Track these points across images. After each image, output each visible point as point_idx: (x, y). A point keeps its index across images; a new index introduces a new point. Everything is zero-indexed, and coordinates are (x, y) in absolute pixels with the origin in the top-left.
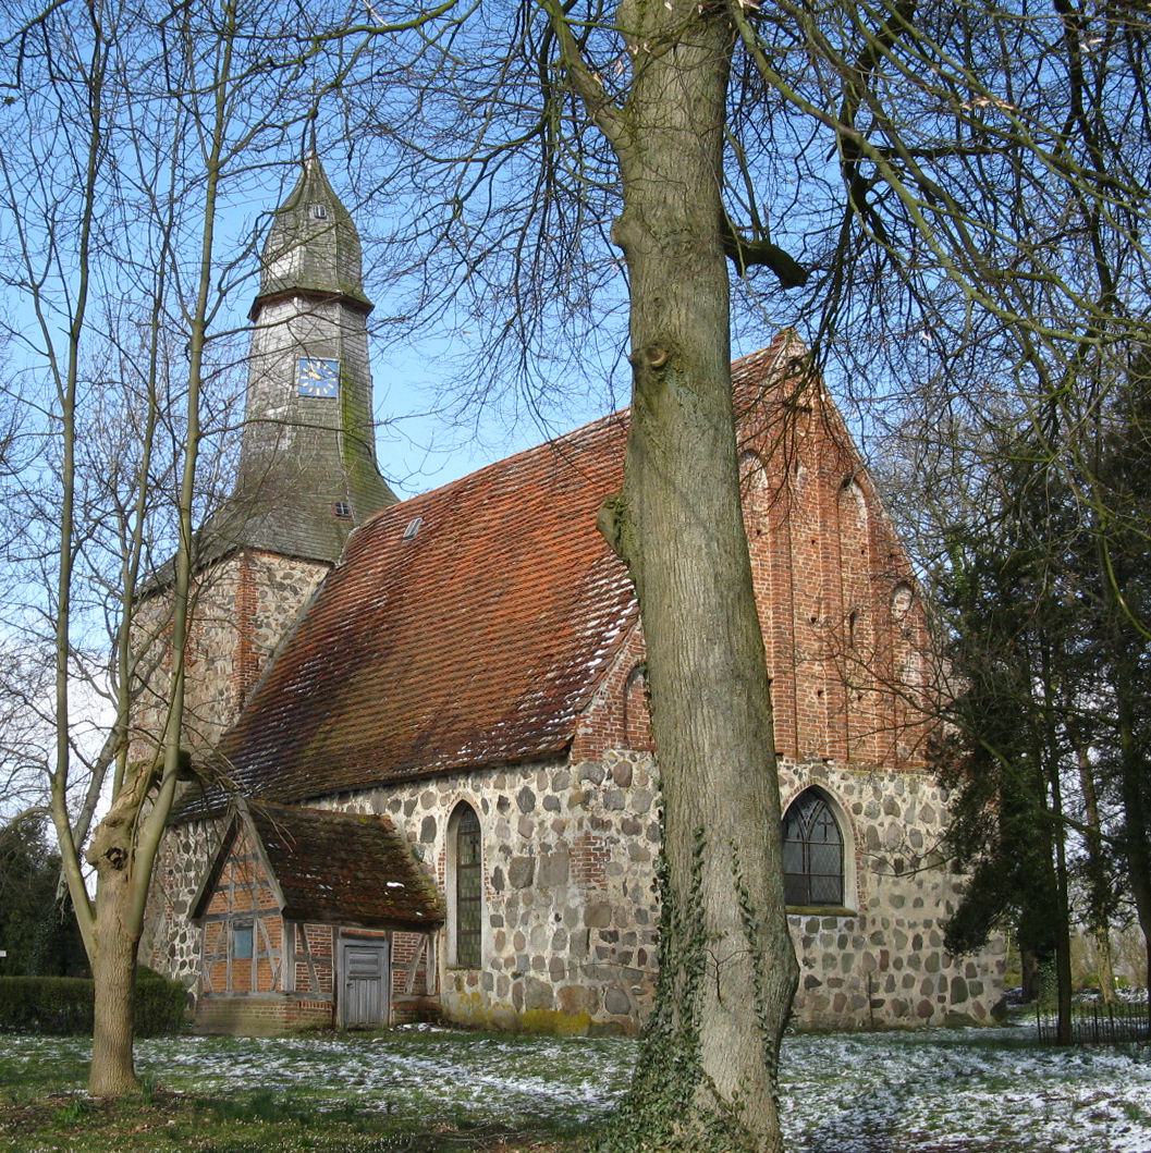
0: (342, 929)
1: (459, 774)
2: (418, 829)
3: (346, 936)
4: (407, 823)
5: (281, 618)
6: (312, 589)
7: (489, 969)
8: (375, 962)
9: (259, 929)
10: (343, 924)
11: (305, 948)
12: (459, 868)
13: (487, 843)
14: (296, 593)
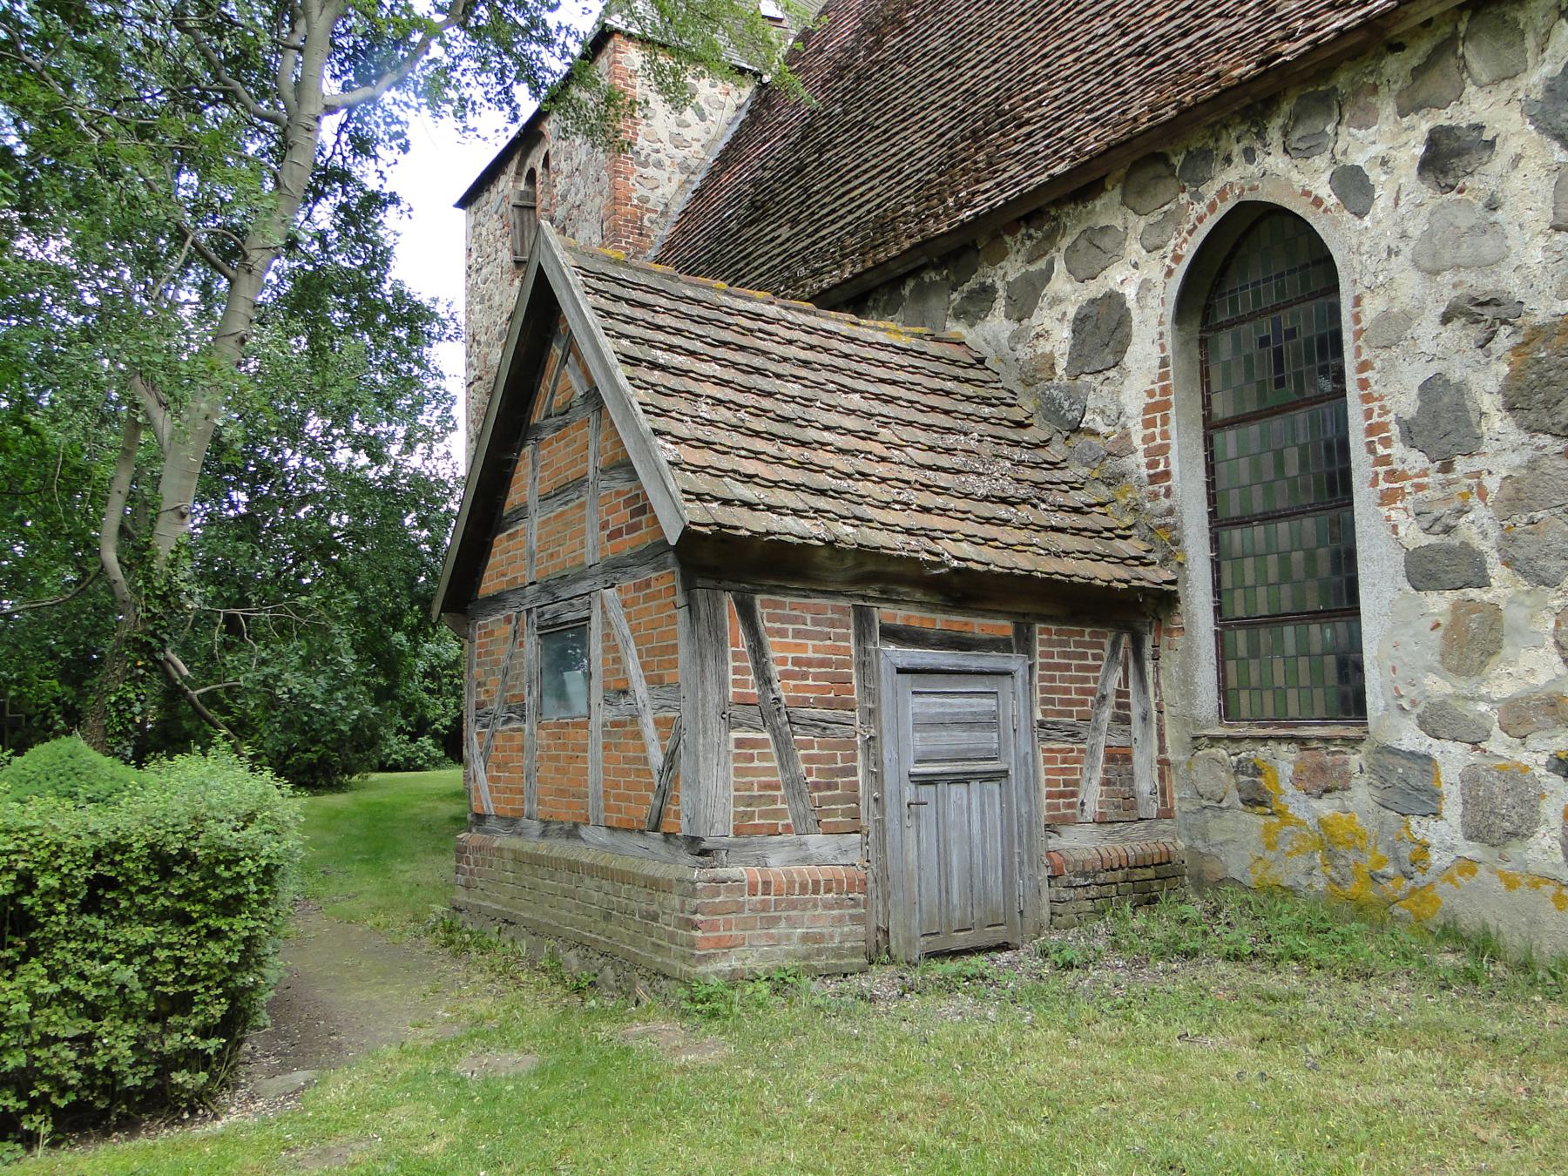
0: (887, 614)
1: (1217, 130)
2: (1059, 341)
3: (893, 634)
4: (1016, 337)
5: (680, 154)
6: (729, 113)
7: (1410, 738)
8: (990, 722)
9: (607, 623)
10: (887, 598)
11: (765, 680)
12: (1211, 427)
13: (1372, 308)
14: (702, 118)
